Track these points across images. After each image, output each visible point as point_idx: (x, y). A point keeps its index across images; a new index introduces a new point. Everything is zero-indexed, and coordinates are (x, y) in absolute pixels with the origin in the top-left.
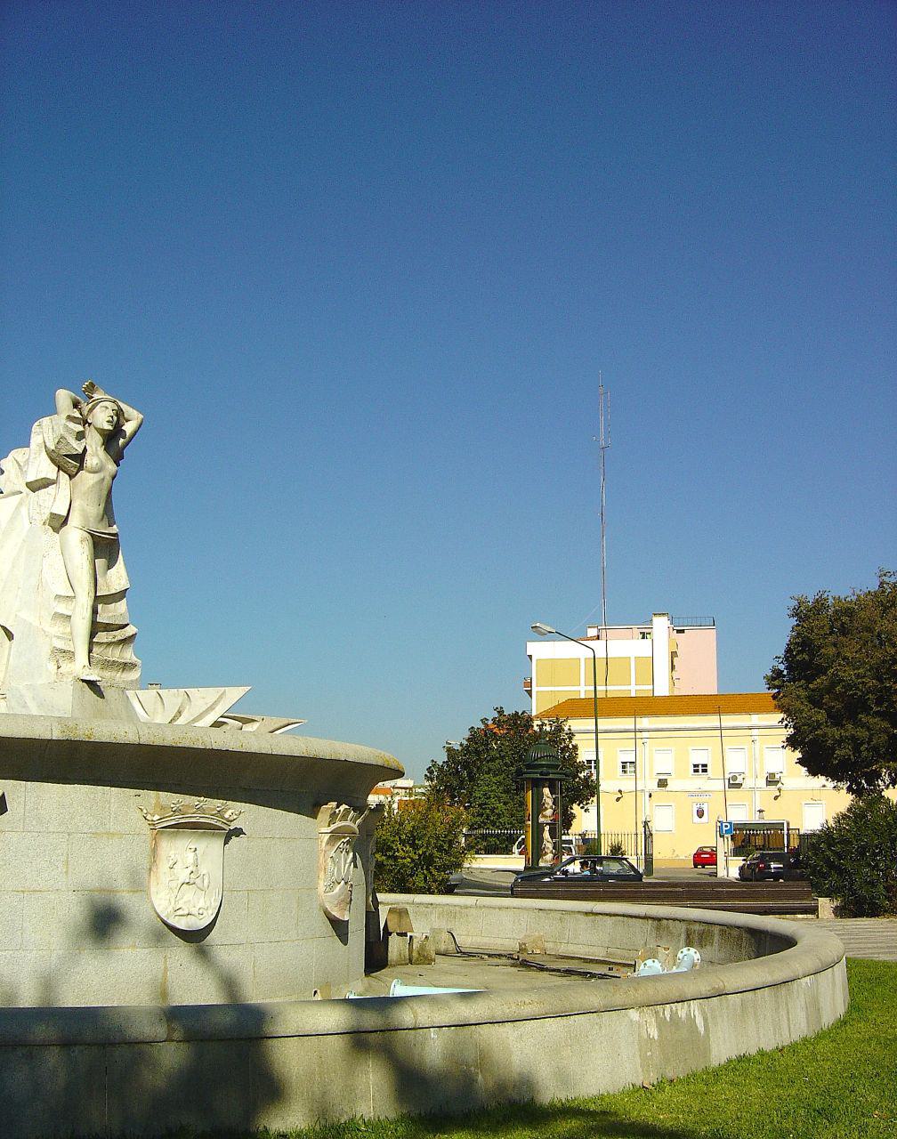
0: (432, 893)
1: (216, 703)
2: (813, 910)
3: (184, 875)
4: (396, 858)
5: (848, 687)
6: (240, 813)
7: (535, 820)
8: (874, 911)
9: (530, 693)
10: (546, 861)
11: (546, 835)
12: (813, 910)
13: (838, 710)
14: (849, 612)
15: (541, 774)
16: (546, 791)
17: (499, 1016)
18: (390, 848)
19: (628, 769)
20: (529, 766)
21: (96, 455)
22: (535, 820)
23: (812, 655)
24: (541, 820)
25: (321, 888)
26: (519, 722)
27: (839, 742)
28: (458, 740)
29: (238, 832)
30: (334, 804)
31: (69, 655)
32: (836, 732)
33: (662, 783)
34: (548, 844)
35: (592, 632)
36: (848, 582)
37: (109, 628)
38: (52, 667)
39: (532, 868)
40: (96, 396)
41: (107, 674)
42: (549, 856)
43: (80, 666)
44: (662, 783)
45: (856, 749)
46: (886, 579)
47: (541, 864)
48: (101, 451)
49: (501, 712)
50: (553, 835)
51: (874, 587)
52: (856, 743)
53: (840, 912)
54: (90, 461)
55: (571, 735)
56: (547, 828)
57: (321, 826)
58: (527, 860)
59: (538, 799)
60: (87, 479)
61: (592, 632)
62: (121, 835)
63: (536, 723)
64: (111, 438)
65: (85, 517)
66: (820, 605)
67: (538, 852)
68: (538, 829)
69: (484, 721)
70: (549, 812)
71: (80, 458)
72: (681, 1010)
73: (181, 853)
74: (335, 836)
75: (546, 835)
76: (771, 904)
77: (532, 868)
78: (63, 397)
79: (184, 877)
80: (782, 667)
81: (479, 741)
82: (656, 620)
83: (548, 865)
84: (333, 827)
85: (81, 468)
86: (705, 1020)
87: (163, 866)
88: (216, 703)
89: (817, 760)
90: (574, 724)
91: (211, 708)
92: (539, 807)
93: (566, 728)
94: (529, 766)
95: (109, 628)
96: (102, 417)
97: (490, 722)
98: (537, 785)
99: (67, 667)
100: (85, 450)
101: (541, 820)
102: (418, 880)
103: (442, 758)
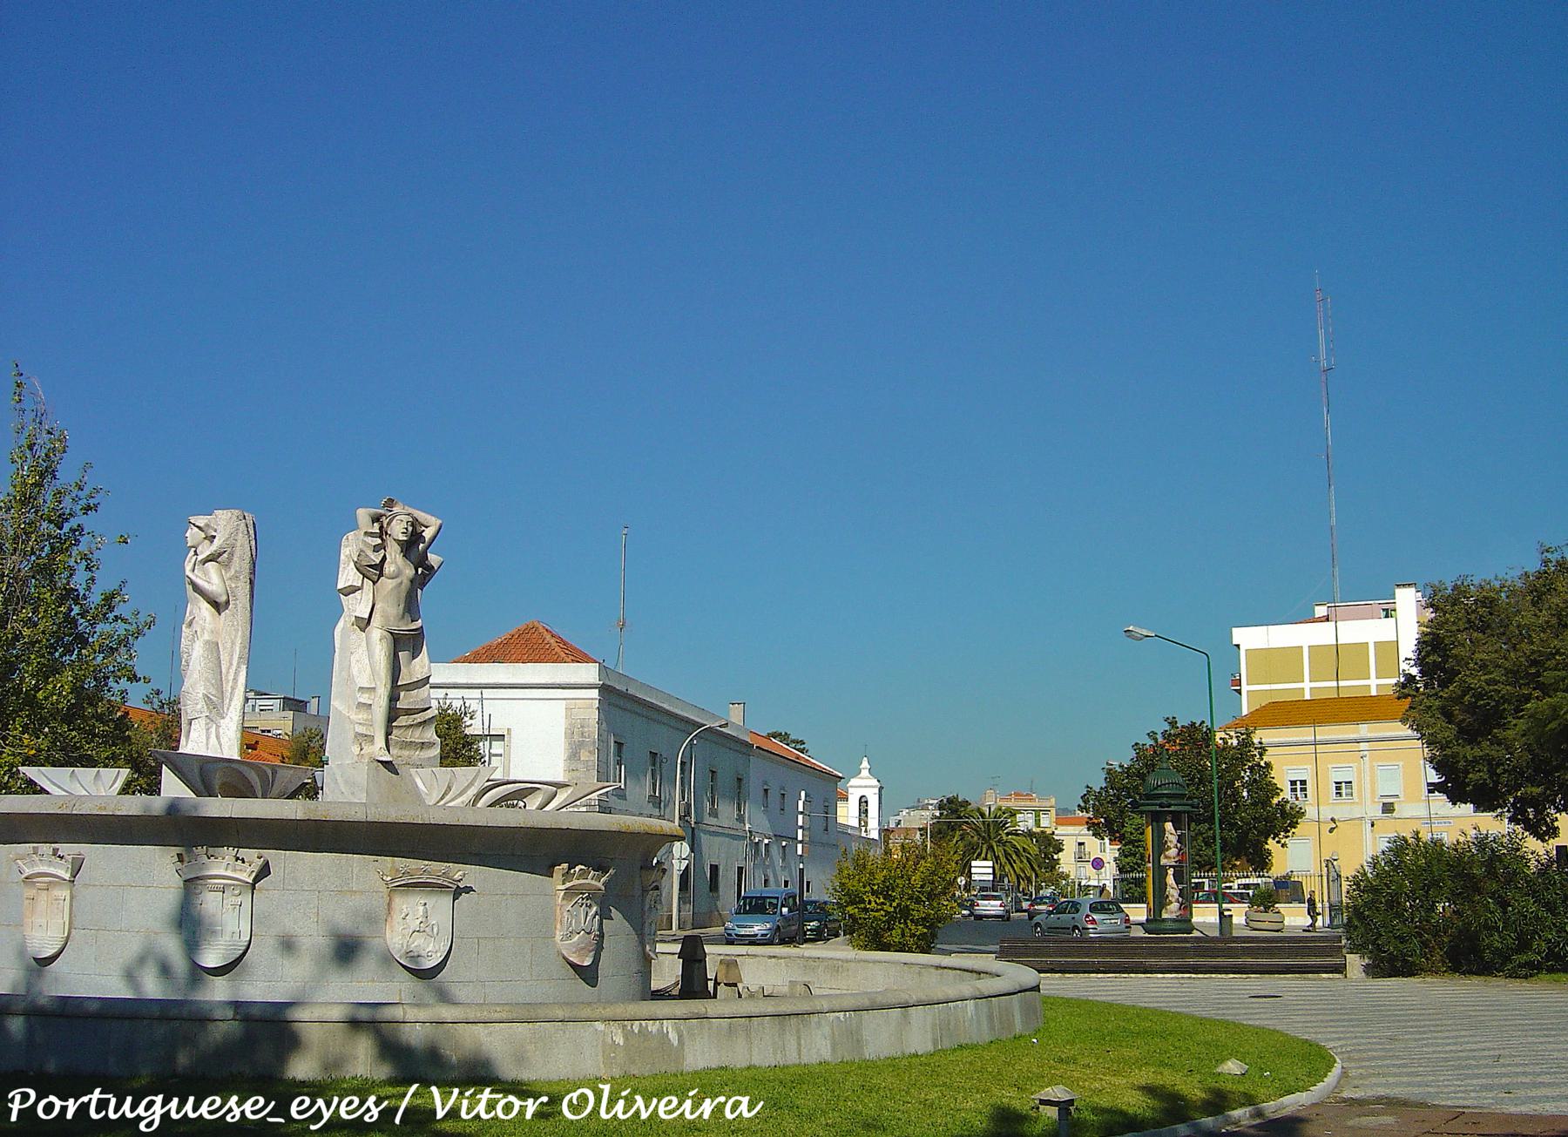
0: (910, 951)
1: (474, 779)
2: (1340, 969)
3: (415, 925)
4: (866, 910)
5: (1479, 696)
6: (462, 873)
7: (1157, 861)
8: (1408, 970)
9: (1239, 692)
10: (1171, 911)
11: (1170, 880)
12: (1340, 969)
13: (1470, 724)
14: (1488, 602)
15: (1161, 805)
16: (1169, 826)
17: (471, 1017)
18: (863, 901)
19: (1343, 791)
20: (1148, 797)
21: (395, 561)
22: (1157, 861)
23: (1445, 658)
24: (1163, 861)
25: (558, 938)
26: (1195, 738)
27: (1475, 761)
28: (1123, 757)
29: (468, 890)
30: (565, 865)
31: (370, 739)
32: (1470, 752)
33: (1388, 808)
34: (1173, 891)
35: (1321, 611)
36: (1504, 563)
37: (409, 712)
38: (356, 749)
39: (1154, 920)
40: (395, 510)
41: (406, 753)
42: (1174, 906)
43: (377, 748)
44: (1388, 808)
45: (1492, 773)
46: (1549, 556)
47: (1165, 916)
48: (400, 558)
49: (1173, 723)
50: (1178, 878)
51: (1534, 566)
52: (1492, 764)
53: (1374, 971)
54: (389, 568)
55: (1263, 750)
56: (1171, 872)
57: (557, 884)
58: (1149, 911)
59: (1160, 834)
60: (387, 584)
61: (1321, 611)
62: (362, 892)
63: (1219, 735)
64: (412, 544)
65: (385, 617)
66: (1460, 591)
67: (1161, 901)
68: (1161, 872)
69: (1152, 735)
70: (1173, 852)
71: (380, 567)
72: (653, 1027)
73: (412, 908)
74: (570, 893)
75: (1170, 880)
76: (1289, 962)
77: (1154, 920)
78: (363, 515)
79: (416, 924)
80: (1414, 671)
81: (1148, 760)
82: (1399, 592)
83: (1174, 916)
84: (568, 885)
85: (381, 575)
86: (680, 1036)
87: (397, 917)
88: (474, 779)
89: (1454, 785)
90: (1261, 736)
91: (471, 784)
92: (1161, 846)
93: (1256, 741)
94: (1148, 797)
95: (409, 712)
96: (398, 530)
97: (1159, 737)
98: (1157, 819)
99: (367, 749)
100: (384, 558)
101: (1163, 861)
102: (895, 936)
103: (1098, 783)
